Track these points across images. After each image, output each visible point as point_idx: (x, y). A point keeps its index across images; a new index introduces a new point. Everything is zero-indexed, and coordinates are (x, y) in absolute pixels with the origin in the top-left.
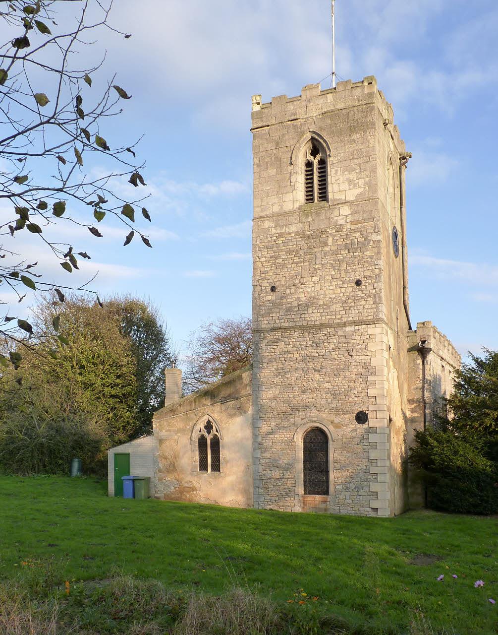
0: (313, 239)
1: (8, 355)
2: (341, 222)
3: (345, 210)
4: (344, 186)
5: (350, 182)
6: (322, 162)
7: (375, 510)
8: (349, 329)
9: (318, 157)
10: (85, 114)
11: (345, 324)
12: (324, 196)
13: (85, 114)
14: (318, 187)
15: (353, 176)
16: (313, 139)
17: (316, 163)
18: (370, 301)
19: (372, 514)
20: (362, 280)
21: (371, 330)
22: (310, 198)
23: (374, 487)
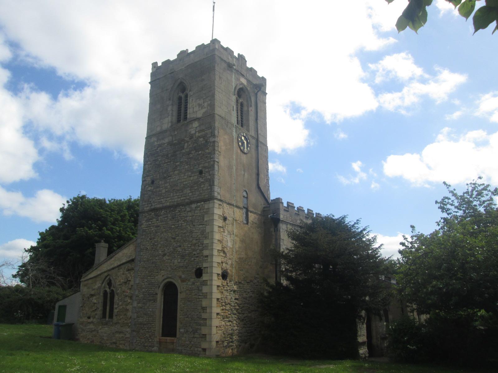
3: (196, 124)
4: (196, 109)
5: (199, 105)
6: (186, 96)
8: (194, 206)
11: (192, 202)
15: (201, 102)
23: (204, 331)
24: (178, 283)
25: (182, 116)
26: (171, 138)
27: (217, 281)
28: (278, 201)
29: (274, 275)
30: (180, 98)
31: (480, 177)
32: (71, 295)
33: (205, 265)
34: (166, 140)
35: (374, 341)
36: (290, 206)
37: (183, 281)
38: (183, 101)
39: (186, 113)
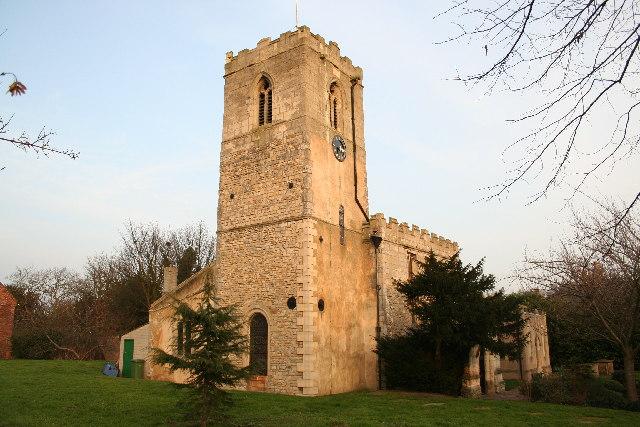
0: (260, 151)
1: (151, 235)
2: (280, 137)
3: (283, 128)
4: (283, 110)
5: (287, 105)
6: (270, 93)
7: (301, 389)
8: (283, 225)
9: (268, 90)
10: (487, 353)
11: (280, 222)
12: (270, 120)
13: (487, 353)
14: (266, 116)
15: (289, 101)
16: (263, 78)
17: (266, 93)
18: (300, 200)
19: (299, 394)
20: (294, 182)
21: (299, 224)
22: (261, 122)
23: (300, 367)
24: (266, 314)
25: (266, 97)
26: (252, 144)
27: (312, 314)
28: (378, 217)
29: (376, 303)
30: (262, 96)
31: (288, 303)
32: (378, 316)
33: (299, 294)
34: (248, 147)
35: (488, 378)
36: (393, 221)
37: (274, 312)
38: (266, 97)
39: (270, 113)
